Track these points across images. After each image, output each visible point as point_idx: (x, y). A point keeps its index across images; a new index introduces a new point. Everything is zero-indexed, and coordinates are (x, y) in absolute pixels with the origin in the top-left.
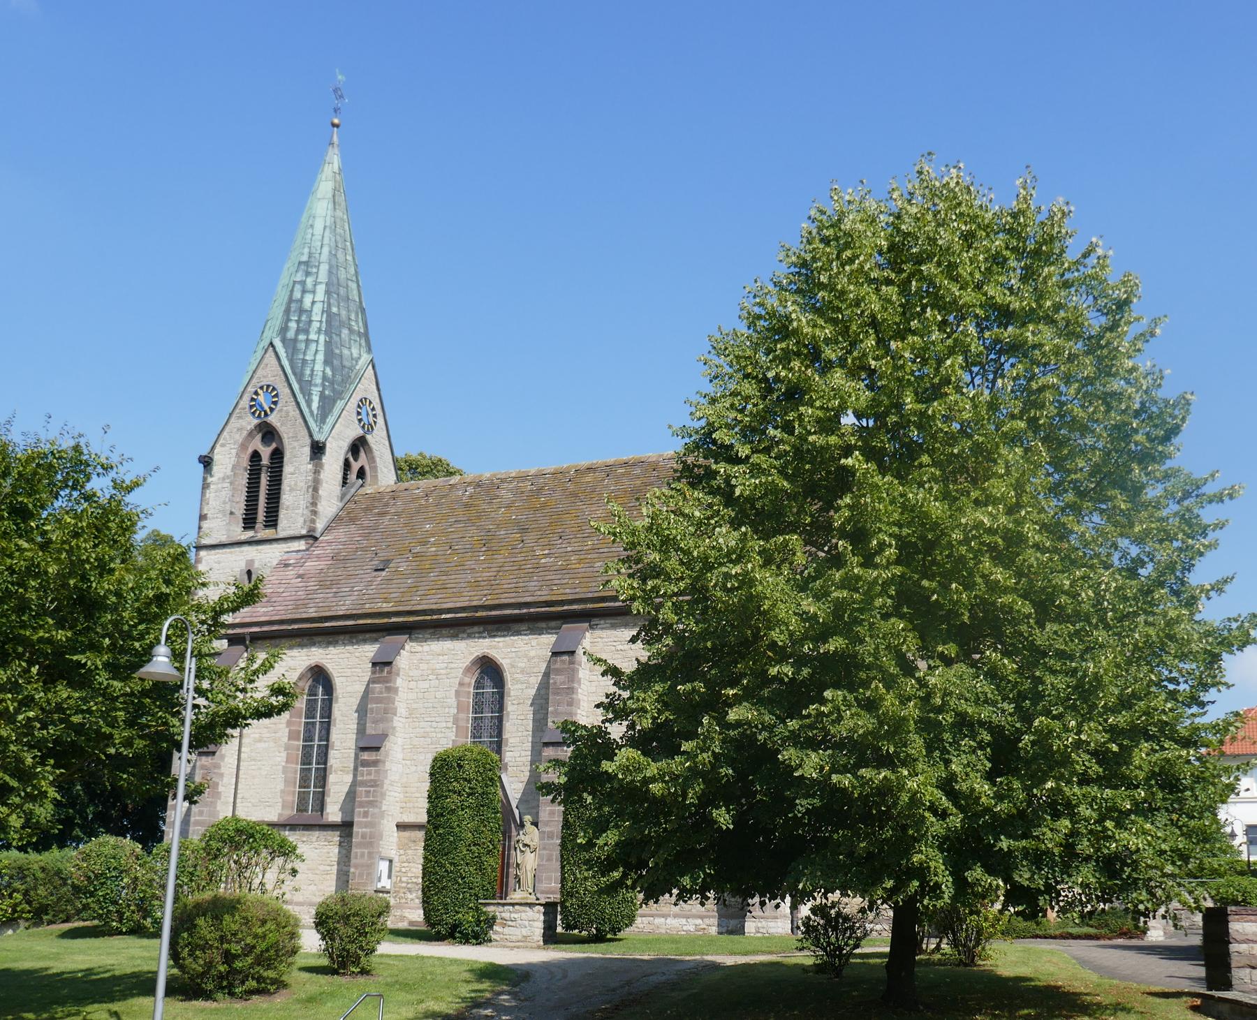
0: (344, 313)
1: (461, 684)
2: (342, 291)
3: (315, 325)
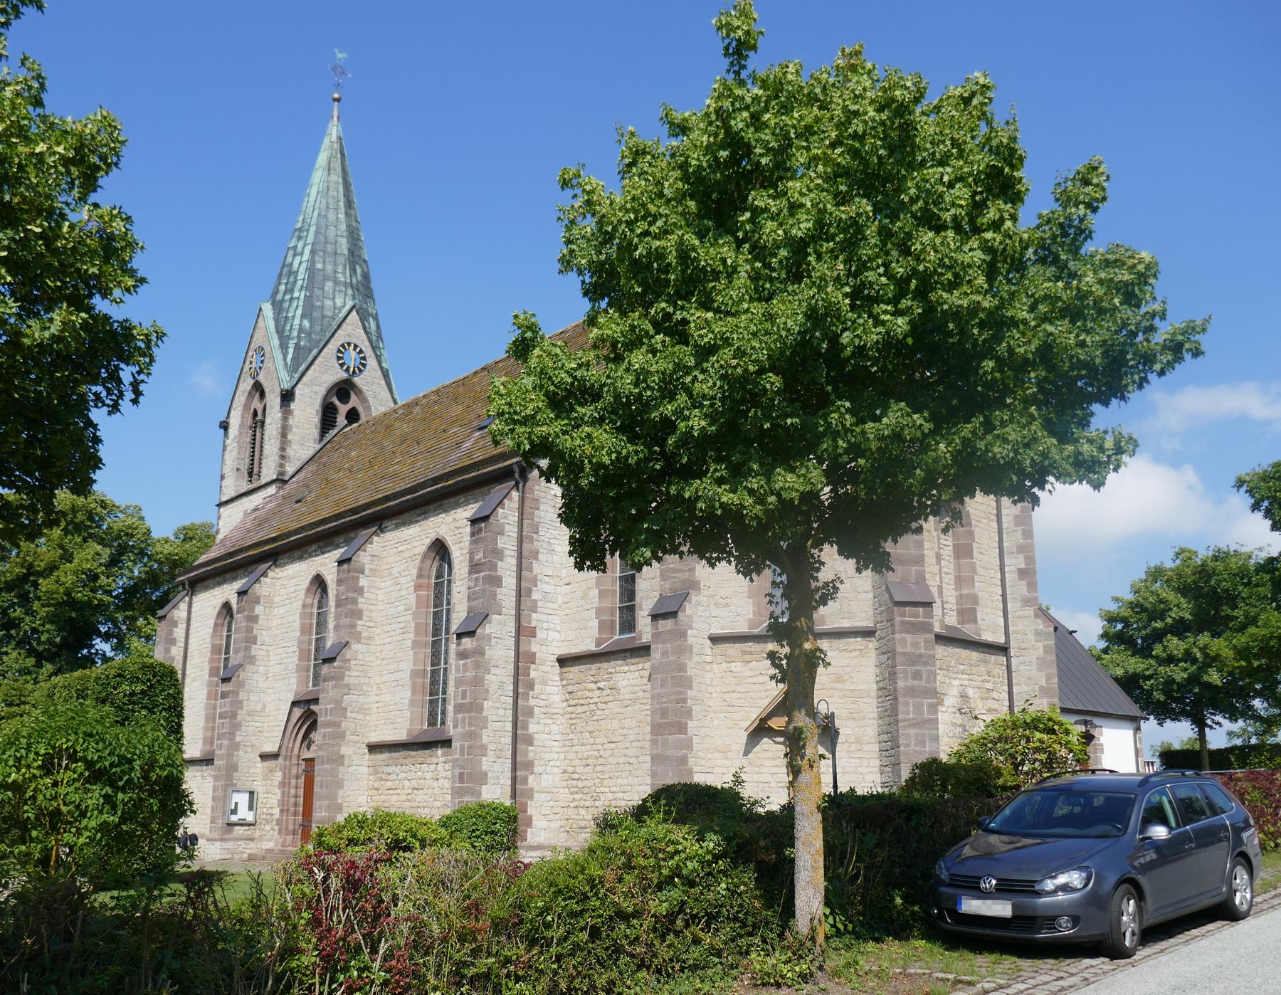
0: (329, 267)
1: (304, 606)
2: (330, 248)
3: (299, 283)
